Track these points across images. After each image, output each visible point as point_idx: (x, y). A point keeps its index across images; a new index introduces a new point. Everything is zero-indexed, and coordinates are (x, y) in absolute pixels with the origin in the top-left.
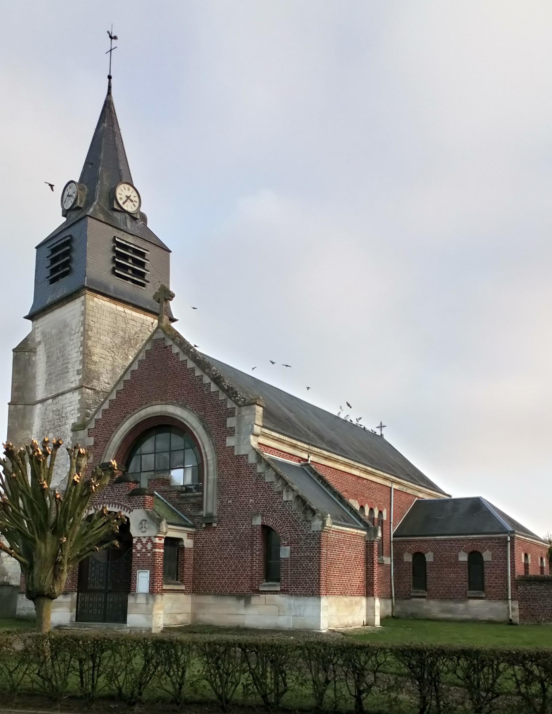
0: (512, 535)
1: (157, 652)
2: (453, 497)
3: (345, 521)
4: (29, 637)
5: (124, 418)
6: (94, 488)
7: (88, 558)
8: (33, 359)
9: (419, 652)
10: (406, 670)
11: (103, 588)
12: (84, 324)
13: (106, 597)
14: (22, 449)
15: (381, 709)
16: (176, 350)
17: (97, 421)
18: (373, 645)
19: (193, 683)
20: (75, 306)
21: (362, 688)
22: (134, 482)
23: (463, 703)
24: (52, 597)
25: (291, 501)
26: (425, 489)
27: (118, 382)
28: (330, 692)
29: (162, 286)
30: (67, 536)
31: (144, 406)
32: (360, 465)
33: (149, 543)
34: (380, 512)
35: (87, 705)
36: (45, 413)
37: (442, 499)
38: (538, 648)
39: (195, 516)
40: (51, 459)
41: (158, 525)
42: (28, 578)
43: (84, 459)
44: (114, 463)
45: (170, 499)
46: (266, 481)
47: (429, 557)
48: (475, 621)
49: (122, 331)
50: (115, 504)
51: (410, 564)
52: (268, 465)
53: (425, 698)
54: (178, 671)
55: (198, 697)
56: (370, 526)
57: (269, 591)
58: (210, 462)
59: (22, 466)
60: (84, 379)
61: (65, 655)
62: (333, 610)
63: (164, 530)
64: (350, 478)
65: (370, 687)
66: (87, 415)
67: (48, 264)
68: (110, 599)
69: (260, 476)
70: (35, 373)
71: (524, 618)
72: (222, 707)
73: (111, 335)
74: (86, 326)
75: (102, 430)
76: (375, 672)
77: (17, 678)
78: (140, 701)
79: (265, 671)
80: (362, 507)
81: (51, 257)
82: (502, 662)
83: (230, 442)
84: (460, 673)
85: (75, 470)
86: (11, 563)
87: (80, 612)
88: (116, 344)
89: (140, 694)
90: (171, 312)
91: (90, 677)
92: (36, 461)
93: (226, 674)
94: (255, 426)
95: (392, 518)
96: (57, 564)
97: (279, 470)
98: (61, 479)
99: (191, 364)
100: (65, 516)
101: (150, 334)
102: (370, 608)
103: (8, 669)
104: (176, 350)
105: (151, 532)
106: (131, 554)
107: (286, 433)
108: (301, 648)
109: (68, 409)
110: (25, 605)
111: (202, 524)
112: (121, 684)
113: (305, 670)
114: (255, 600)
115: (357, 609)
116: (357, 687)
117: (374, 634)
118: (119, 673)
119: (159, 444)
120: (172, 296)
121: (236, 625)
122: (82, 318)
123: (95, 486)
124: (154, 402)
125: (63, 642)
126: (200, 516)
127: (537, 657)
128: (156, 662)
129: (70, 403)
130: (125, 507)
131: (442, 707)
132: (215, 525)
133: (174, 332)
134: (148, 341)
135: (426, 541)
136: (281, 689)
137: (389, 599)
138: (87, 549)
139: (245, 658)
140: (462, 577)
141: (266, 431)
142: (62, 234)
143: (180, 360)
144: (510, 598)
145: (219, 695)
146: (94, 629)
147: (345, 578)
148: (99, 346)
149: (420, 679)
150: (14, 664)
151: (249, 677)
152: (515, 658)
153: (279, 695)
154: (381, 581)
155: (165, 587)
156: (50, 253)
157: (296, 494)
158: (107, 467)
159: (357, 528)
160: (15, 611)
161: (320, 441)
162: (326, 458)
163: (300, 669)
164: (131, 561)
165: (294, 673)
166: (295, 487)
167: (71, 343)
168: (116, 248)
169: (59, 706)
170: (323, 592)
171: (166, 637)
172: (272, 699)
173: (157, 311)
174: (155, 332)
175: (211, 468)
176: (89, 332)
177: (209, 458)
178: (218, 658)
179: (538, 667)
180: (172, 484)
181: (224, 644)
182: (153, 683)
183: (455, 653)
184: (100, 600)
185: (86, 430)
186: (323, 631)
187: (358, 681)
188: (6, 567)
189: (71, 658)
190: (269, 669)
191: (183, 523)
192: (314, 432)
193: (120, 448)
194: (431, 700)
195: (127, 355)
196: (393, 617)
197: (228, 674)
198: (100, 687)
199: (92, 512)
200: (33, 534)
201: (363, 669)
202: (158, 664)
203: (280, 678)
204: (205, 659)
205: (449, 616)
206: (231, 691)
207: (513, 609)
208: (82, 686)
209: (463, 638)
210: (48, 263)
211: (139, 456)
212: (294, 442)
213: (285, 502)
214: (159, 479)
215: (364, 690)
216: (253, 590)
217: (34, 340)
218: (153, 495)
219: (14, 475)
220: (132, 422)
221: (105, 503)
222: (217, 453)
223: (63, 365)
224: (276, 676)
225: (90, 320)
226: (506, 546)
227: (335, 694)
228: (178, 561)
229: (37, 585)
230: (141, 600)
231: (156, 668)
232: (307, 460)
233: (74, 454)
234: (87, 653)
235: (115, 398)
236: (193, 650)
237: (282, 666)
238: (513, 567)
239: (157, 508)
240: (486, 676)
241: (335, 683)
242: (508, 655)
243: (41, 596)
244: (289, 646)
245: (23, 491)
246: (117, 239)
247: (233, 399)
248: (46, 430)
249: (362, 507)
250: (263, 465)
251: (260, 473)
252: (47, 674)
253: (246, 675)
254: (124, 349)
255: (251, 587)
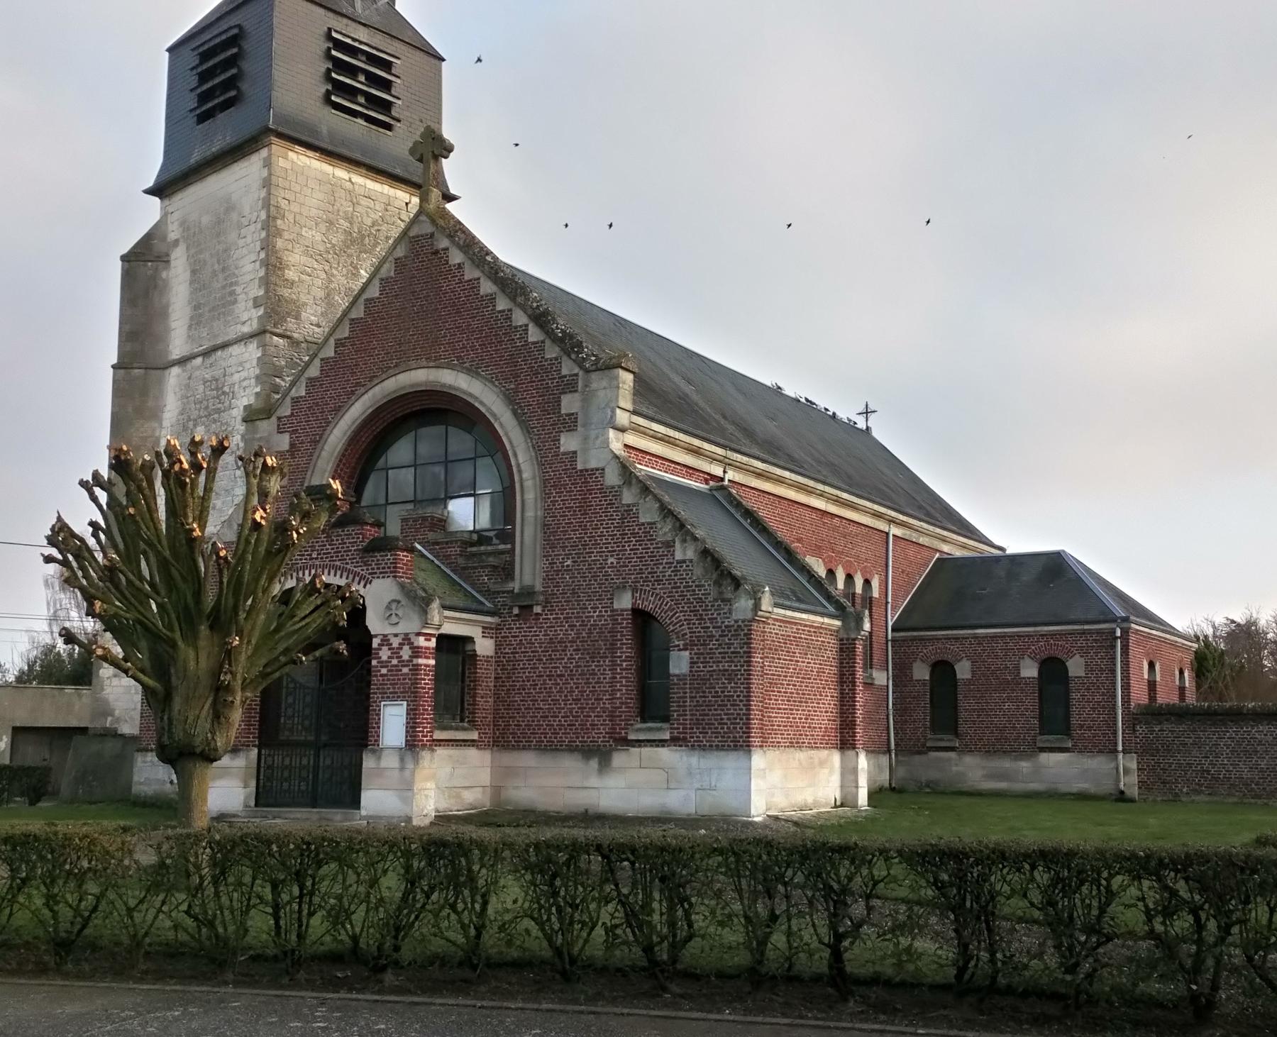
0: (1125, 625)
1: (430, 864)
2: (1008, 552)
3: (799, 600)
4: (168, 838)
5: (352, 395)
6: (295, 535)
7: (280, 678)
8: (164, 275)
9: (955, 855)
10: (930, 892)
11: (311, 738)
12: (267, 204)
13: (317, 756)
14: (147, 457)
15: (878, 968)
16: (456, 257)
17: (296, 401)
18: (866, 843)
19: (504, 924)
20: (247, 172)
21: (841, 930)
22: (372, 525)
23: (1040, 955)
24: (210, 757)
25: (691, 561)
26: (955, 537)
27: (340, 320)
28: (778, 939)
29: (428, 128)
30: (240, 633)
31: (391, 372)
32: (828, 489)
33: (406, 648)
34: (867, 582)
35: (288, 973)
36: (188, 386)
37: (987, 555)
38: (1187, 846)
39: (498, 593)
40: (207, 479)
41: (424, 612)
42: (162, 719)
43: (273, 479)
44: (336, 485)
45: (446, 558)
46: (642, 520)
47: (963, 670)
48: (1051, 796)
49: (346, 219)
50: (336, 568)
51: (924, 685)
52: (645, 490)
53: (966, 946)
54: (473, 902)
55: (514, 953)
56: (847, 609)
57: (648, 741)
58: (529, 484)
59: (147, 492)
60: (268, 316)
61: (243, 874)
62: (775, 777)
63: (436, 620)
64: (807, 512)
65: (858, 926)
66: (276, 389)
67: (194, 83)
68: (326, 760)
69: (629, 511)
70: (167, 306)
71: (1149, 789)
72: (564, 974)
73: (323, 227)
74: (272, 209)
75: (308, 420)
76: (868, 897)
77: (144, 921)
78: (396, 963)
79: (648, 897)
80: (831, 573)
81: (199, 70)
82: (1118, 873)
83: (568, 443)
84: (1035, 896)
85: (255, 500)
86: (121, 690)
87: (264, 786)
88: (334, 246)
89: (397, 949)
90: (444, 182)
91: (295, 916)
92: (176, 482)
93: (571, 906)
94: (618, 411)
95: (891, 594)
96: (220, 691)
97: (666, 498)
98: (223, 519)
99: (487, 287)
100: (236, 593)
101: (403, 225)
102: (849, 773)
103: (126, 904)
104: (456, 257)
105: (409, 624)
106: (368, 670)
107: (681, 425)
108: (721, 851)
109: (236, 377)
110: (151, 774)
111: (511, 608)
112: (358, 930)
113: (730, 895)
114: (618, 759)
115: (825, 772)
116: (833, 927)
117: (856, 823)
118: (353, 907)
119: (424, 449)
120: (447, 149)
121: (582, 810)
122: (263, 194)
123: (298, 533)
124: (413, 364)
125: (234, 848)
126: (508, 592)
127: (1184, 864)
128: (429, 885)
129: (241, 364)
130: (356, 574)
131: (999, 964)
132: (538, 609)
133: (452, 222)
134: (398, 241)
135: (956, 638)
136: (681, 934)
137: (884, 753)
138: (283, 659)
139: (610, 871)
140: (1027, 710)
141: (641, 421)
142: (222, 23)
143: (466, 278)
144: (1120, 748)
145: (557, 948)
146: (296, 821)
147: (799, 714)
148: (298, 249)
149: (957, 908)
150: (137, 893)
151: (616, 910)
152: (1144, 866)
153: (676, 947)
154: (869, 719)
155: (438, 735)
156: (197, 62)
157: (700, 547)
158: (321, 494)
159: (822, 615)
160: (130, 788)
161: (747, 442)
162: (760, 475)
163: (718, 895)
164: (369, 684)
165: (706, 902)
166: (699, 533)
167: (241, 243)
168: (334, 53)
169: (230, 976)
170: (756, 741)
171: (448, 833)
172: (663, 954)
173: (416, 179)
174: (415, 221)
175: (530, 496)
176: (279, 222)
177: (525, 476)
178: (554, 876)
179: (1187, 882)
180: (453, 528)
181: (567, 847)
182: (423, 928)
183: (1026, 856)
184: (305, 762)
185: (274, 419)
186: (756, 819)
187: (835, 915)
188: (111, 698)
189: (254, 879)
190: (656, 895)
191: (474, 606)
192: (734, 423)
193: (343, 455)
194: (979, 949)
195: (355, 268)
196: (892, 789)
197: (575, 907)
198: (313, 938)
199: (290, 583)
200: (172, 630)
201: (845, 891)
202: (432, 889)
203: (680, 913)
204: (528, 877)
205: (1002, 785)
206: (581, 942)
207: (1126, 771)
208: (278, 933)
209: (1034, 829)
210: (194, 81)
211: (384, 473)
212: (697, 442)
213: (678, 562)
214: (424, 519)
215: (847, 932)
216: (615, 740)
217: (164, 238)
218: (412, 550)
219: (132, 511)
220: (368, 404)
221: (316, 567)
222: (541, 464)
223: (224, 287)
224: (671, 909)
225: (280, 198)
226: (1114, 647)
227: (789, 942)
228: (463, 681)
229: (179, 734)
230: (390, 761)
231: (428, 897)
232: (722, 479)
233: (251, 463)
234: (289, 868)
235: (332, 354)
236: (504, 859)
237: (684, 887)
238: (1126, 687)
239: (421, 576)
240: (1087, 901)
241: (789, 920)
242: (1129, 859)
243: (186, 755)
244: (697, 849)
245: (149, 544)
246: (334, 34)
247: (573, 356)
248: (189, 419)
249: (831, 573)
250: (635, 489)
251: (628, 505)
252: (206, 912)
253: (610, 907)
254: (350, 256)
255: (612, 733)
